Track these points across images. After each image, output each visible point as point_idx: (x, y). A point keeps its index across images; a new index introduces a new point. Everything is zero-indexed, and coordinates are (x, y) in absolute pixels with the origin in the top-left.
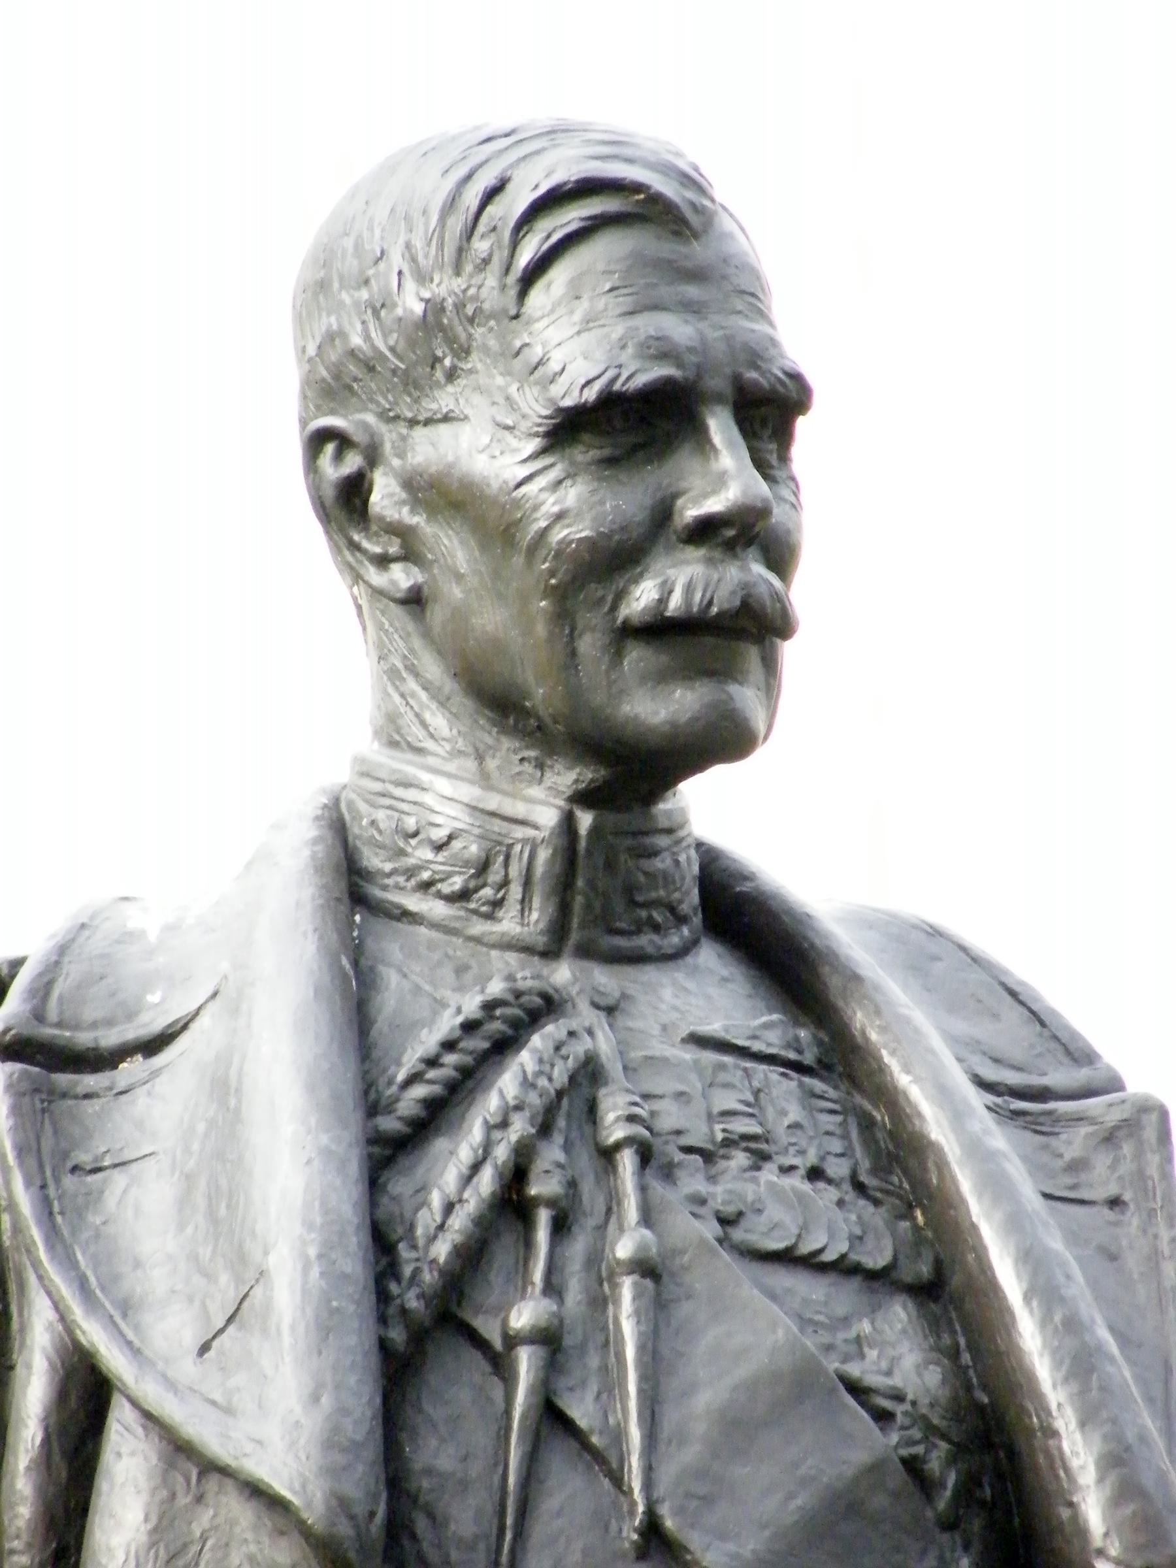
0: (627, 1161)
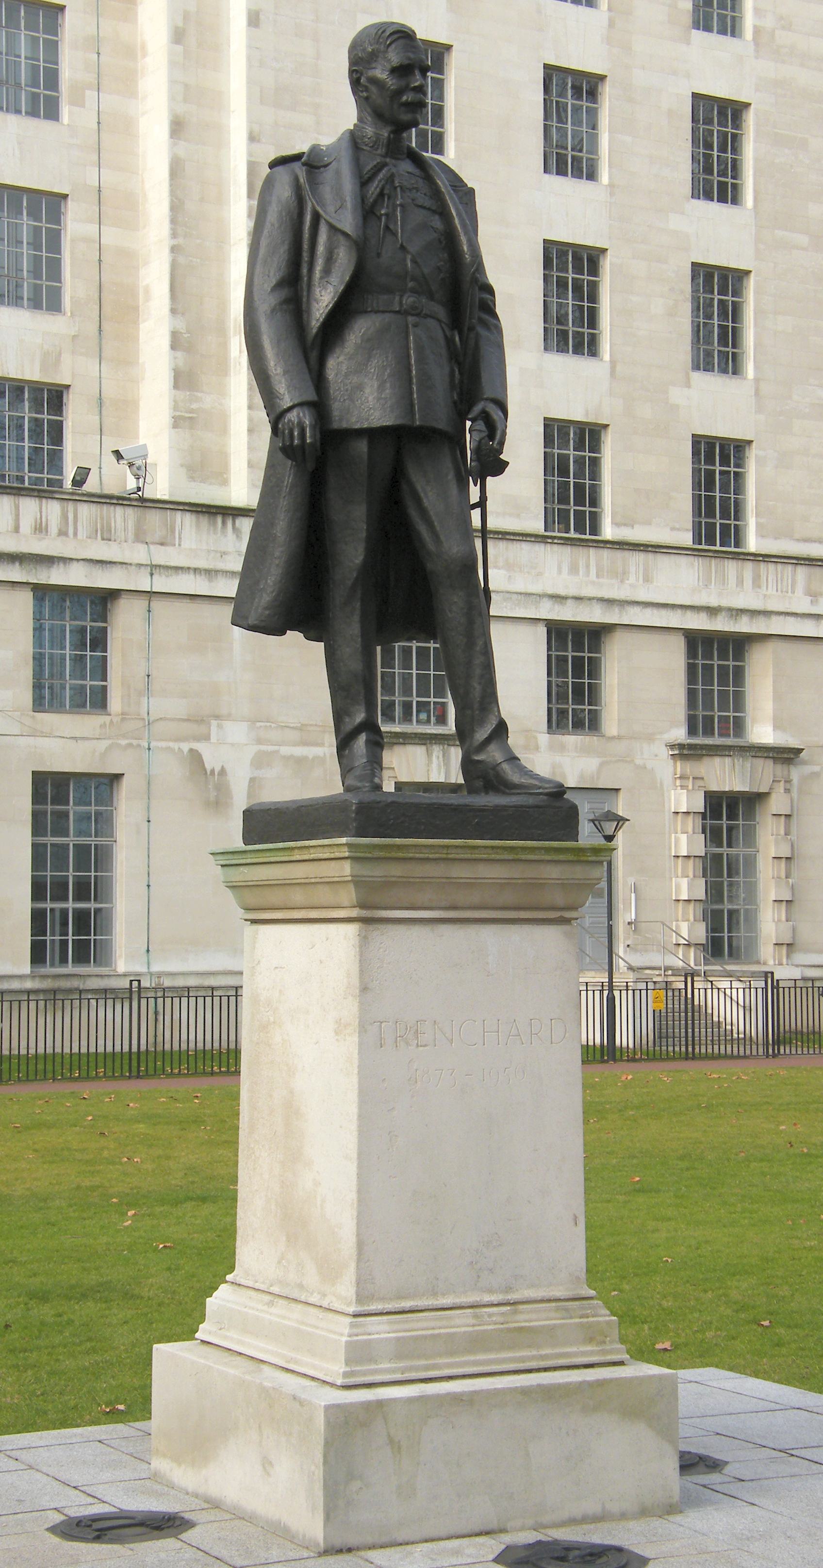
0: (399, 189)
